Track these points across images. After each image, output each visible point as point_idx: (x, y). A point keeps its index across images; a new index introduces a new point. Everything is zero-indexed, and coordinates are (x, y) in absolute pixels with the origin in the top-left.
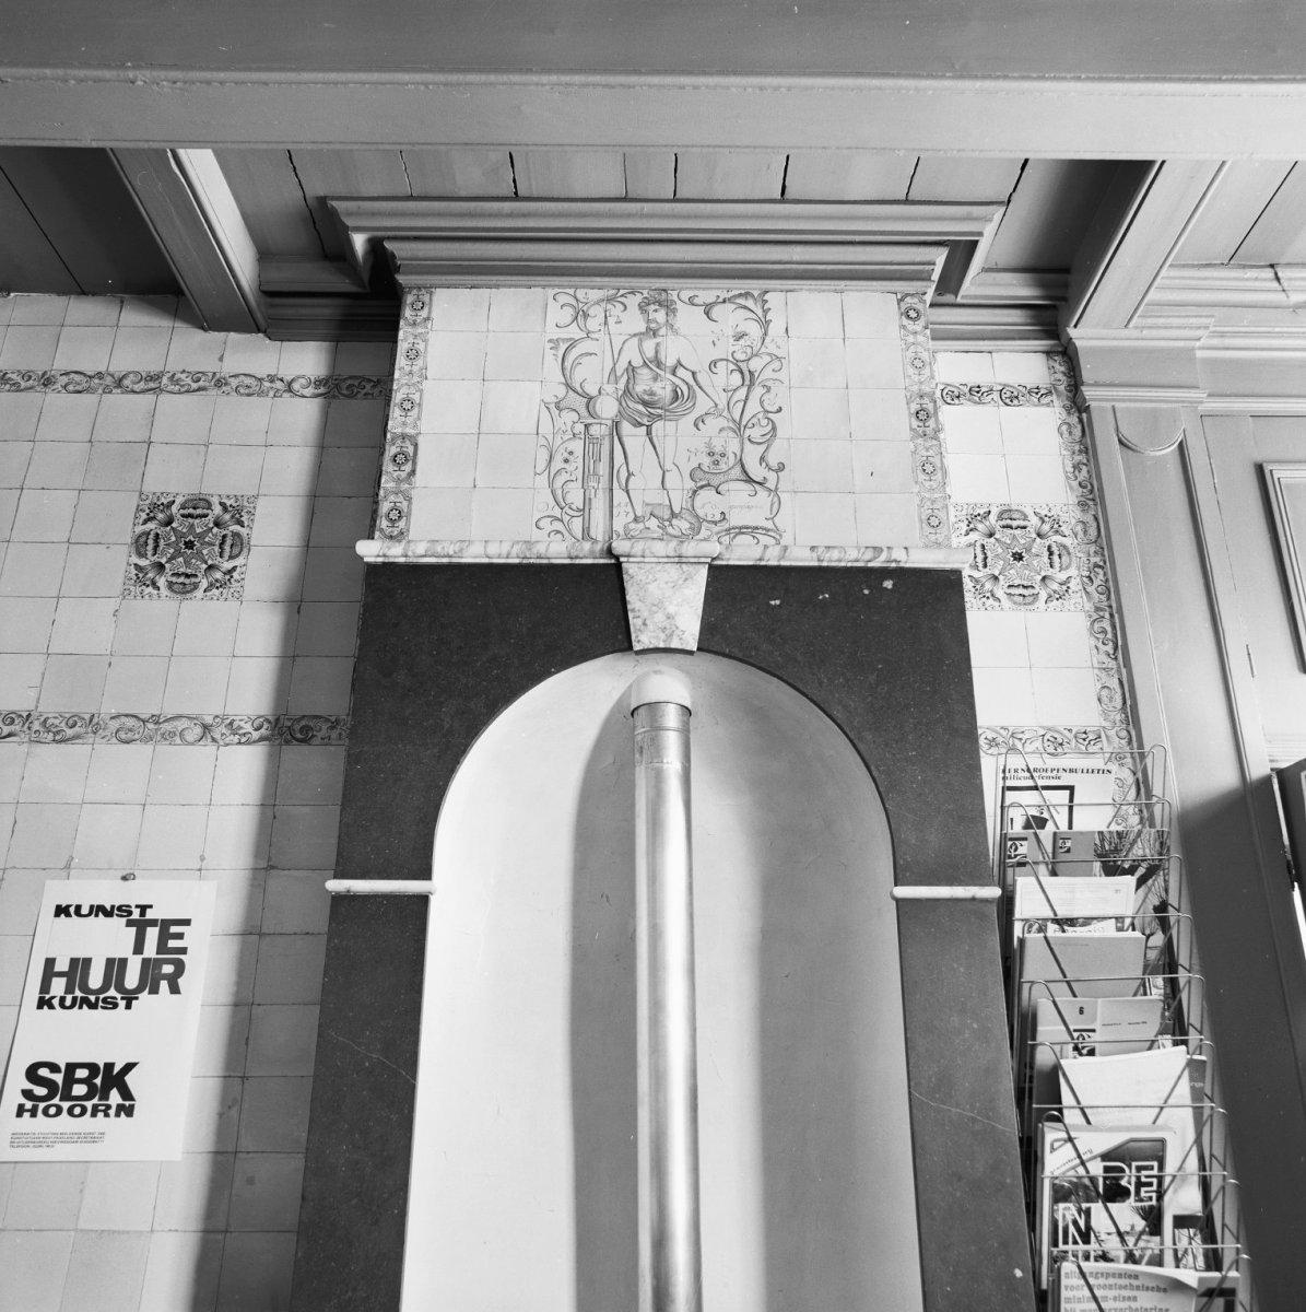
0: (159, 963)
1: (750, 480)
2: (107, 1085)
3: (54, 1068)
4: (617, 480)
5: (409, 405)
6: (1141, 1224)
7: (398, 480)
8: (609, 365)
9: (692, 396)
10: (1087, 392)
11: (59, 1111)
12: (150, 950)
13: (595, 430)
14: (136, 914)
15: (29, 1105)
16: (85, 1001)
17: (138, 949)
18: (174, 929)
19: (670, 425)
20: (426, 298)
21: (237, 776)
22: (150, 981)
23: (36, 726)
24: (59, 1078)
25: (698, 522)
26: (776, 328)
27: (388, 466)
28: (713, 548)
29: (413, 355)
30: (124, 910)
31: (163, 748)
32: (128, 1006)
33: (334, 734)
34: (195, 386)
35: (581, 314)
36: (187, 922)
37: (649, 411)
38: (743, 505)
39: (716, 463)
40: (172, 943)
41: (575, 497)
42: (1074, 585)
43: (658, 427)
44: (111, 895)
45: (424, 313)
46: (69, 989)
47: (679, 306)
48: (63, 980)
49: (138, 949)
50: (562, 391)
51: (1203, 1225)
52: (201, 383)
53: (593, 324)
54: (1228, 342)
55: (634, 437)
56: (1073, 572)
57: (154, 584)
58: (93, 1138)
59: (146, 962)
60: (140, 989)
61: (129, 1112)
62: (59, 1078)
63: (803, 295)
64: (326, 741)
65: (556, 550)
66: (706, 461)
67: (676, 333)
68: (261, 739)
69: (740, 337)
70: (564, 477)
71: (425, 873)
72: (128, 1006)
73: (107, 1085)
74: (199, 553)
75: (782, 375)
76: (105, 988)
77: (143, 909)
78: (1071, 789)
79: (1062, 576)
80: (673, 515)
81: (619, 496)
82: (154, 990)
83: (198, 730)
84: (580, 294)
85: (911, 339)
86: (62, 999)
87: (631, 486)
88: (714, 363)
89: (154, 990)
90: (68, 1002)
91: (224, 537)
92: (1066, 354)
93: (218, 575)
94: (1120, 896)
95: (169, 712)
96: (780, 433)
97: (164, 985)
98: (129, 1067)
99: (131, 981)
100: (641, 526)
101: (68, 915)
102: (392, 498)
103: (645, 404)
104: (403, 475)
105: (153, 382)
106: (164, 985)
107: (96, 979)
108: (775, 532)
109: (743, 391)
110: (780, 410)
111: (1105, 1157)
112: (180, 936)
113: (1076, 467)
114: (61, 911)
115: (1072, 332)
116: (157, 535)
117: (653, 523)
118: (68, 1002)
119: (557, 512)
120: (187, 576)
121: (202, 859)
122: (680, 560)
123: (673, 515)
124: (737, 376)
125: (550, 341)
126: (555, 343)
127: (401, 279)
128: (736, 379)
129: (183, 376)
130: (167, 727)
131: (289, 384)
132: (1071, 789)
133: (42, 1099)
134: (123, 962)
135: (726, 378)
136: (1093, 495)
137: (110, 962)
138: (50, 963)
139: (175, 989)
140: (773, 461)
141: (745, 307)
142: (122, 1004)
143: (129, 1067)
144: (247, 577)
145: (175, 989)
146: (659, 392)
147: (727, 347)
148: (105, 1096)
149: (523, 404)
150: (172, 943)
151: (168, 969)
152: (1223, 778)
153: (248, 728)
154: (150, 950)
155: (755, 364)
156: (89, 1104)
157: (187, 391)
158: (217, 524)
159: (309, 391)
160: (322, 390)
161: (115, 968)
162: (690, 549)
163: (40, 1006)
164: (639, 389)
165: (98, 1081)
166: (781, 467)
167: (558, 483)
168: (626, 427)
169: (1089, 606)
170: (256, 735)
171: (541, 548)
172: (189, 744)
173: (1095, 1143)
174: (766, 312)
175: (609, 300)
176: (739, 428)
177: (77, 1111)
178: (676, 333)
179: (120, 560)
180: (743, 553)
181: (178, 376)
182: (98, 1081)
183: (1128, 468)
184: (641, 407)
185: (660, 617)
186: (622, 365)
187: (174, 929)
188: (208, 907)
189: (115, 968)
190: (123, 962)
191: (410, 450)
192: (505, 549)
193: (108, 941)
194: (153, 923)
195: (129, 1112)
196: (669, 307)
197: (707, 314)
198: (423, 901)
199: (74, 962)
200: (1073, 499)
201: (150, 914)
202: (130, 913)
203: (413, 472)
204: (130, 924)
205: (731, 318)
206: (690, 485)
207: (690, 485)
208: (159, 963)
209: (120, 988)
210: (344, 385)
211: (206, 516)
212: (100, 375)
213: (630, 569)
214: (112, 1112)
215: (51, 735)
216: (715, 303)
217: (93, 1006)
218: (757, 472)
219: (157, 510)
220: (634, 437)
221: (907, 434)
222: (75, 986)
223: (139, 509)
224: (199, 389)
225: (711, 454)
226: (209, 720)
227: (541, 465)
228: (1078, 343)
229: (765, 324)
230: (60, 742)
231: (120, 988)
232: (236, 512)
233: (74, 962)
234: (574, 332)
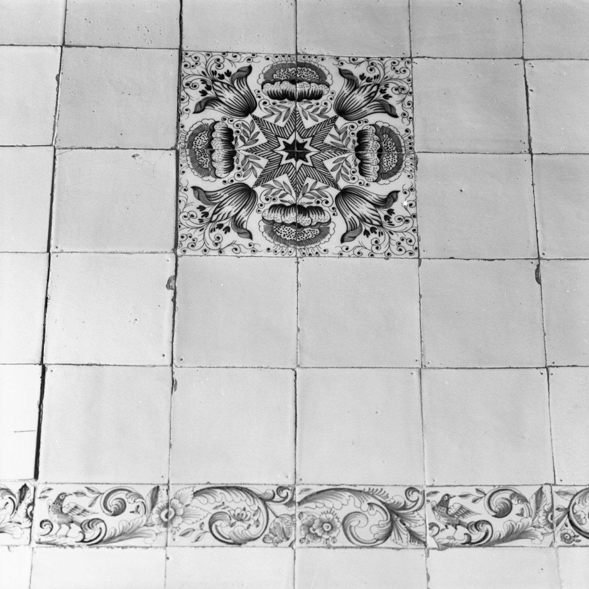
57: (238, 225)
83: (379, 517)
91: (319, 210)
116: (229, 133)
120: (303, 210)
158: (342, 112)
211: (318, 96)
230: (92, 543)
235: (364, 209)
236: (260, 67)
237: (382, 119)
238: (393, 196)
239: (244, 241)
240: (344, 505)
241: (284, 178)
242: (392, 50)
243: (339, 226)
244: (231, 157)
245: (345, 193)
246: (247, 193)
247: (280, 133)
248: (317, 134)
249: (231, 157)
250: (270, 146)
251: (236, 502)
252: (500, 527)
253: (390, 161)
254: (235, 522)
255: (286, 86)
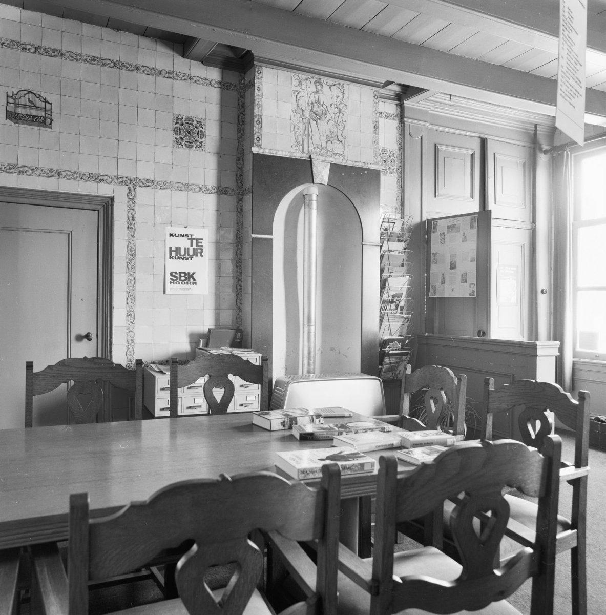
0: (197, 249)
1: (339, 140)
2: (189, 277)
3: (176, 273)
4: (309, 137)
5: (259, 106)
6: (395, 307)
7: (258, 129)
8: (307, 101)
9: (326, 114)
10: (406, 120)
11: (179, 283)
12: (194, 245)
13: (304, 121)
14: (190, 237)
15: (172, 282)
16: (181, 258)
17: (192, 246)
18: (199, 241)
19: (322, 122)
20: (261, 70)
21: (210, 201)
22: (195, 253)
23: (155, 184)
24: (178, 275)
25: (328, 151)
26: (346, 96)
27: (255, 124)
28: (332, 160)
29: (259, 89)
30: (187, 236)
31: (190, 193)
32: (191, 259)
33: (233, 193)
34: (183, 78)
35: (300, 83)
36: (202, 239)
37: (317, 117)
38: (336, 147)
39: (331, 134)
40: (199, 244)
41: (300, 140)
42: (395, 170)
43: (319, 122)
44: (183, 232)
45: (261, 75)
46: (176, 255)
47: (324, 84)
48: (175, 252)
49: (192, 246)
50: (296, 107)
51: (402, 309)
52: (185, 77)
53: (303, 87)
54: (436, 109)
55: (313, 123)
56: (395, 167)
57: (181, 144)
58: (188, 289)
59: (194, 249)
60: (193, 255)
61: (196, 284)
62: (178, 275)
63: (352, 86)
64: (231, 195)
65: (298, 155)
66: (329, 134)
67: (323, 93)
68: (215, 193)
69: (338, 97)
70: (298, 134)
71: (271, 234)
72: (191, 259)
73: (189, 277)
74: (192, 136)
75: (346, 111)
76: (185, 254)
77: (191, 235)
78: (395, 223)
79: (393, 168)
80: (322, 148)
81: (310, 140)
82: (197, 256)
83: (198, 189)
84: (300, 76)
85: (375, 105)
86: (175, 257)
87: (313, 139)
88: (331, 104)
89: (197, 256)
90: (177, 258)
91: (198, 131)
92: (401, 106)
93: (198, 143)
94: (402, 246)
95: (191, 182)
96: (345, 128)
97: (199, 254)
98: (194, 273)
99: (191, 253)
100: (315, 150)
101: (173, 236)
102: (257, 134)
103: (316, 114)
104: (259, 127)
105: (171, 75)
106: (199, 254)
107: (182, 252)
108: (343, 155)
109: (338, 114)
110: (346, 121)
111: (393, 296)
112: (201, 243)
113: (399, 139)
114: (171, 235)
115: (405, 102)
116: (180, 128)
117: (318, 150)
118: (177, 258)
119: (296, 144)
120: (190, 143)
121: (204, 223)
122: (325, 161)
123: (322, 148)
124: (336, 109)
125: (293, 91)
126: (294, 91)
127: (255, 63)
128: (336, 110)
129: (180, 74)
130: (190, 187)
131: (210, 82)
132: (395, 223)
133: (175, 280)
134: (188, 248)
135: (333, 110)
136: (402, 147)
137: (185, 248)
138: (171, 248)
139: (202, 256)
140: (344, 136)
141: (339, 88)
142: (190, 258)
143: (194, 273)
144: (206, 144)
145: (202, 256)
146: (319, 111)
147: (335, 100)
148: (189, 280)
149: (287, 109)
150: (199, 244)
151: (199, 251)
152: (417, 220)
153: (211, 189)
154: (194, 245)
155: (341, 106)
156: (186, 282)
157: (181, 80)
158: (196, 127)
159: (216, 85)
160: (220, 86)
161: (187, 250)
162: (328, 159)
163: (170, 259)
164: (315, 109)
165: (187, 276)
166: (345, 138)
167: (296, 135)
168: (311, 120)
169: (397, 176)
170: (213, 191)
171: (295, 154)
172: (196, 192)
173: (391, 293)
174: (344, 90)
175: (307, 79)
176: (337, 125)
177: (183, 283)
178: (323, 93)
179: (170, 136)
180: (338, 161)
181: (178, 74)
182: (187, 276)
183: (410, 140)
184: (315, 115)
185: (320, 176)
186: (310, 102)
187: (199, 241)
188: (206, 234)
189: (187, 250)
190: (188, 248)
191: (260, 120)
192: (287, 153)
193: (184, 243)
194: (194, 239)
195: (196, 284)
196: (321, 84)
197: (330, 88)
198: (272, 240)
199: (176, 248)
200: (397, 148)
201: (193, 237)
202: (188, 236)
203: (261, 127)
204: (189, 239)
205: (336, 91)
206: (326, 140)
207: (326, 140)
208: (197, 249)
209: (189, 255)
210: (226, 85)
211: (192, 124)
212: (153, 69)
213: (314, 162)
214: (192, 283)
215: (160, 187)
216: (332, 85)
217: (183, 259)
218: (340, 138)
219: (178, 120)
220: (313, 123)
221: (372, 132)
222: (176, 254)
223: (173, 119)
224: (184, 80)
225: (330, 132)
226: (201, 186)
227: (292, 129)
228: (405, 105)
229: (343, 94)
230: (162, 189)
231: (189, 255)
232: (201, 124)
233: (176, 248)
234: (298, 89)
235: (198, 143)
236: (184, 118)
237: (201, 129)
238: (202, 142)
239: (182, 147)
240: (25, 169)
241: (187, 137)
242: (203, 117)
243: (195, 146)
244: (180, 132)
245: (196, 140)
246: (182, 139)
247: (186, 134)
248: (192, 130)
249: (180, 132)
250: (186, 132)
251: (180, 185)
252: (50, 175)
253: (202, 136)
254: (295, 438)
255: (188, 122)
